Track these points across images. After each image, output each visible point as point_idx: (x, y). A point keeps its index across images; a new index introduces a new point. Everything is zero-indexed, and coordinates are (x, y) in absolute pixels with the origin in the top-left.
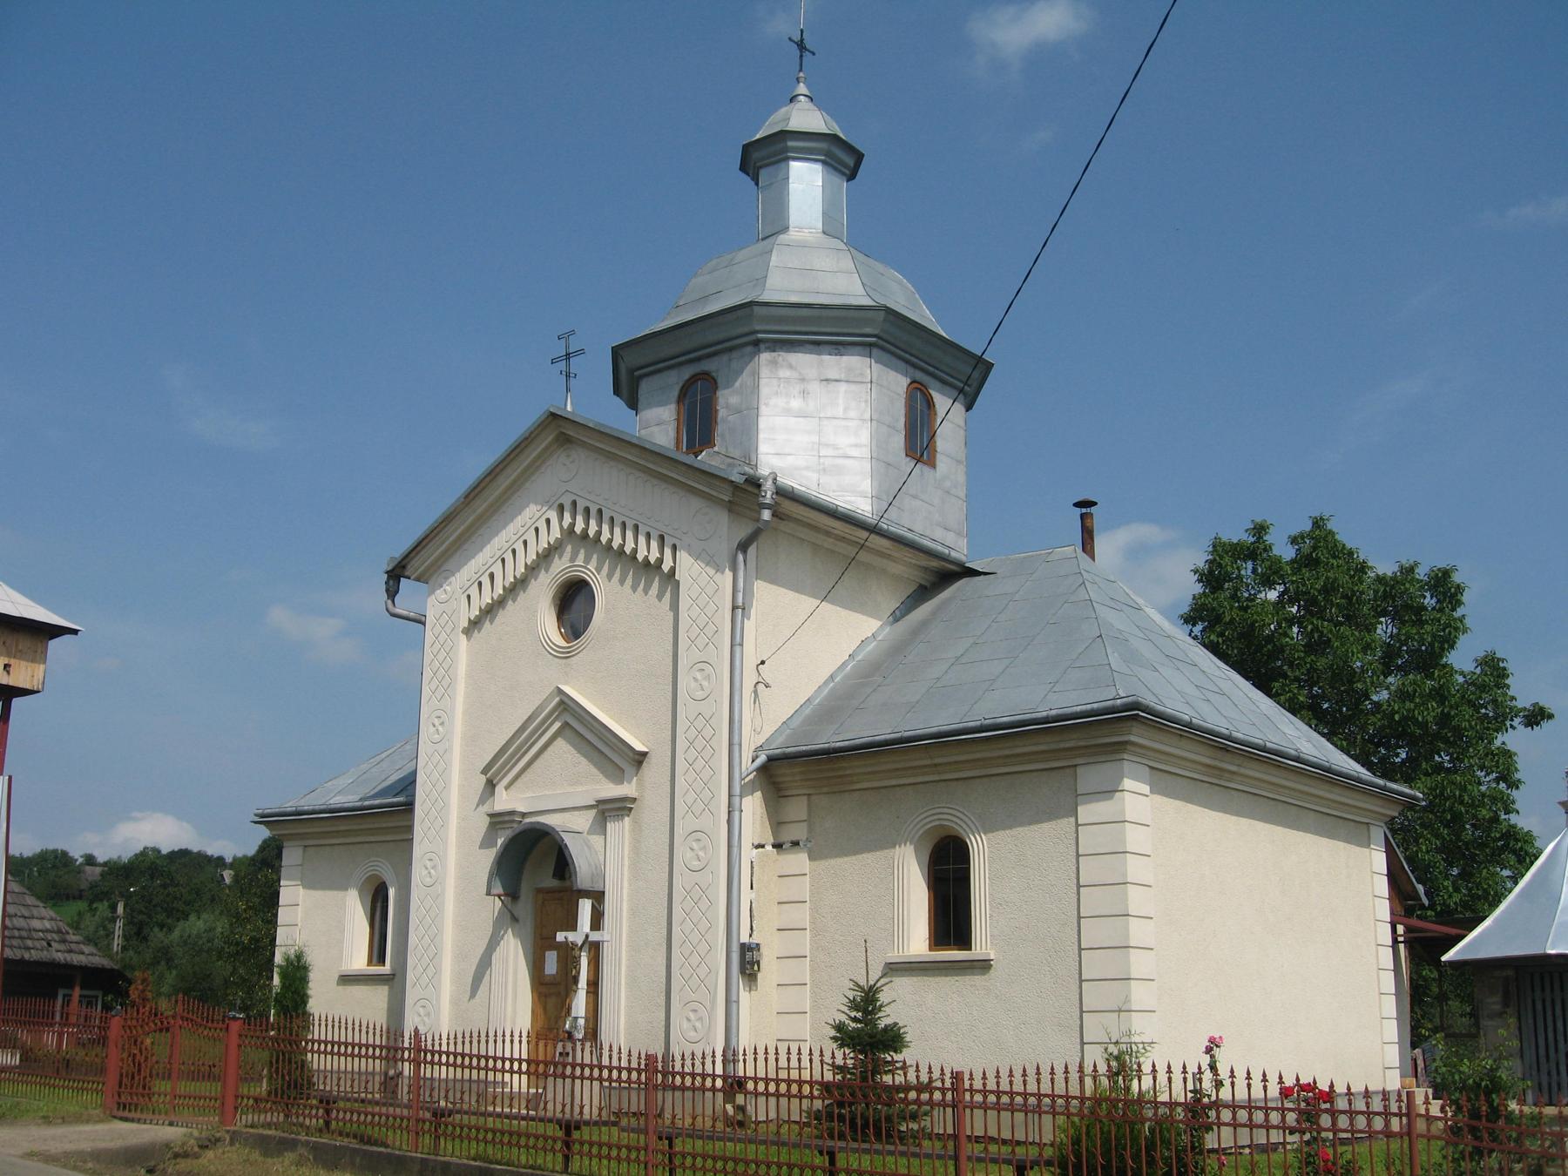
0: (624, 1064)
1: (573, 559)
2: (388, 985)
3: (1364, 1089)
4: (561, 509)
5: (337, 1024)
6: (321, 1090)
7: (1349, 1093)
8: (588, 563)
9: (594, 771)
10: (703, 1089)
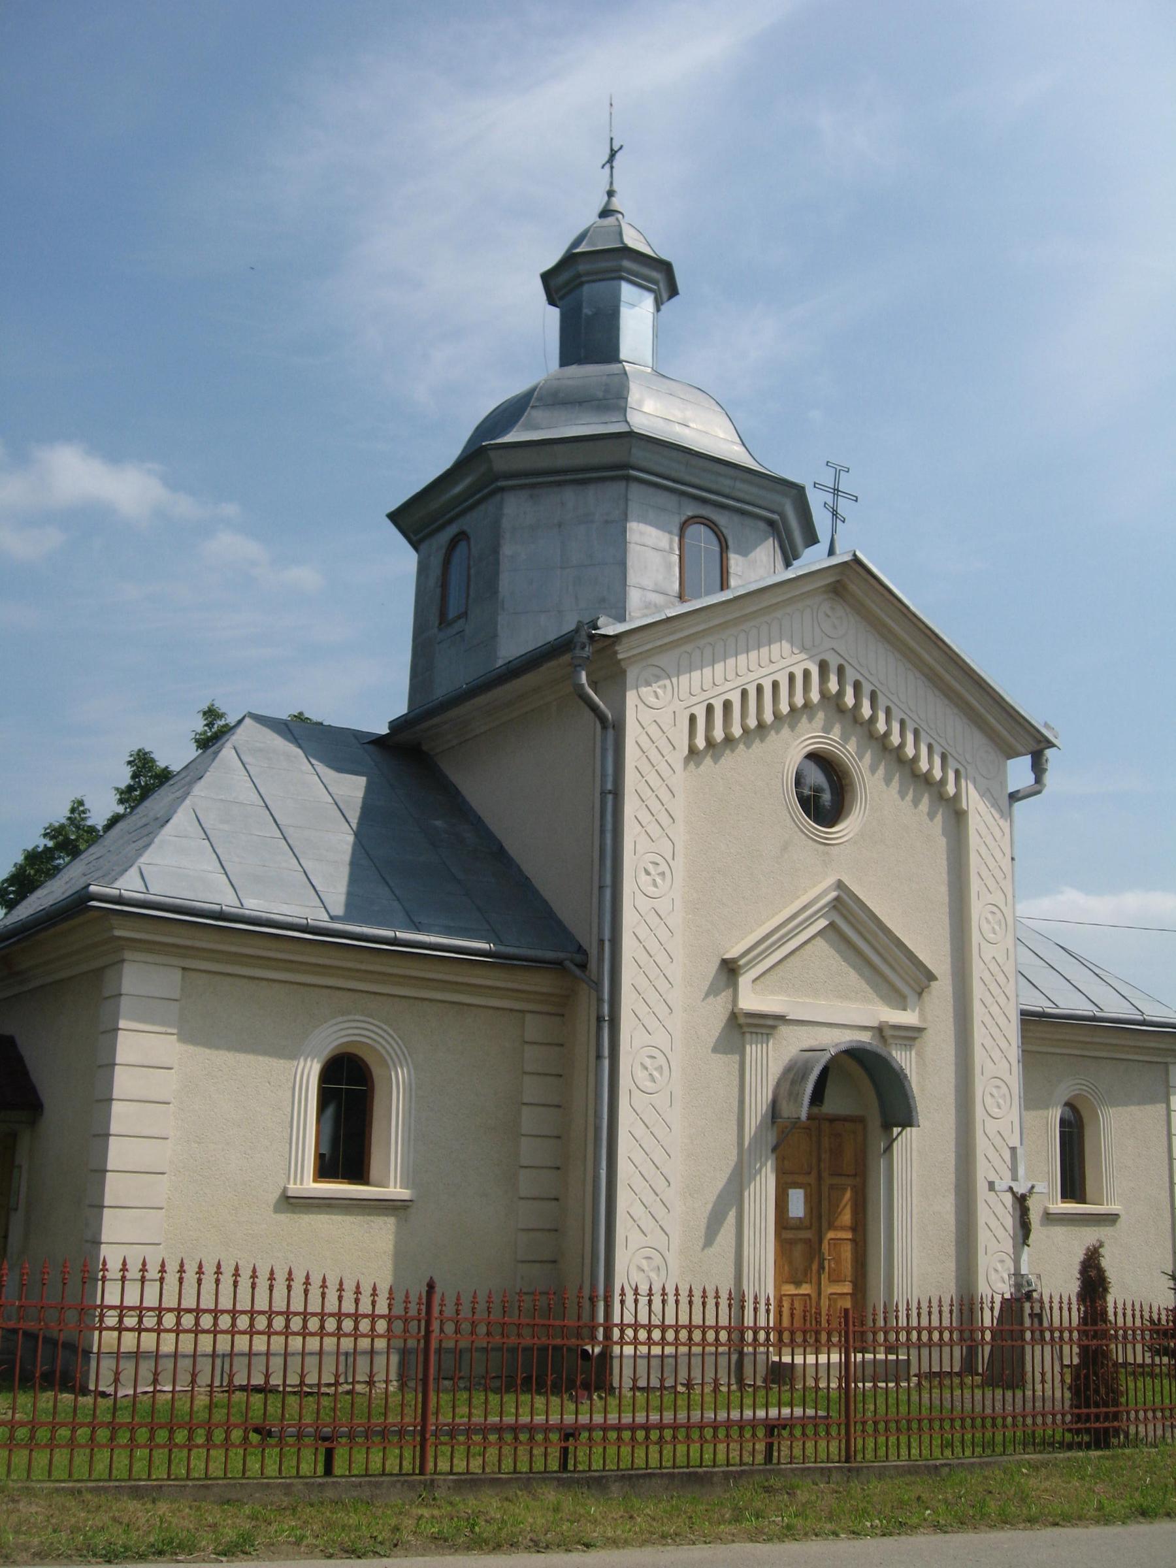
0: (348, 1307)
4: (823, 667)
5: (1065, 1307)
8: (847, 743)
9: (864, 985)
10: (930, 1344)
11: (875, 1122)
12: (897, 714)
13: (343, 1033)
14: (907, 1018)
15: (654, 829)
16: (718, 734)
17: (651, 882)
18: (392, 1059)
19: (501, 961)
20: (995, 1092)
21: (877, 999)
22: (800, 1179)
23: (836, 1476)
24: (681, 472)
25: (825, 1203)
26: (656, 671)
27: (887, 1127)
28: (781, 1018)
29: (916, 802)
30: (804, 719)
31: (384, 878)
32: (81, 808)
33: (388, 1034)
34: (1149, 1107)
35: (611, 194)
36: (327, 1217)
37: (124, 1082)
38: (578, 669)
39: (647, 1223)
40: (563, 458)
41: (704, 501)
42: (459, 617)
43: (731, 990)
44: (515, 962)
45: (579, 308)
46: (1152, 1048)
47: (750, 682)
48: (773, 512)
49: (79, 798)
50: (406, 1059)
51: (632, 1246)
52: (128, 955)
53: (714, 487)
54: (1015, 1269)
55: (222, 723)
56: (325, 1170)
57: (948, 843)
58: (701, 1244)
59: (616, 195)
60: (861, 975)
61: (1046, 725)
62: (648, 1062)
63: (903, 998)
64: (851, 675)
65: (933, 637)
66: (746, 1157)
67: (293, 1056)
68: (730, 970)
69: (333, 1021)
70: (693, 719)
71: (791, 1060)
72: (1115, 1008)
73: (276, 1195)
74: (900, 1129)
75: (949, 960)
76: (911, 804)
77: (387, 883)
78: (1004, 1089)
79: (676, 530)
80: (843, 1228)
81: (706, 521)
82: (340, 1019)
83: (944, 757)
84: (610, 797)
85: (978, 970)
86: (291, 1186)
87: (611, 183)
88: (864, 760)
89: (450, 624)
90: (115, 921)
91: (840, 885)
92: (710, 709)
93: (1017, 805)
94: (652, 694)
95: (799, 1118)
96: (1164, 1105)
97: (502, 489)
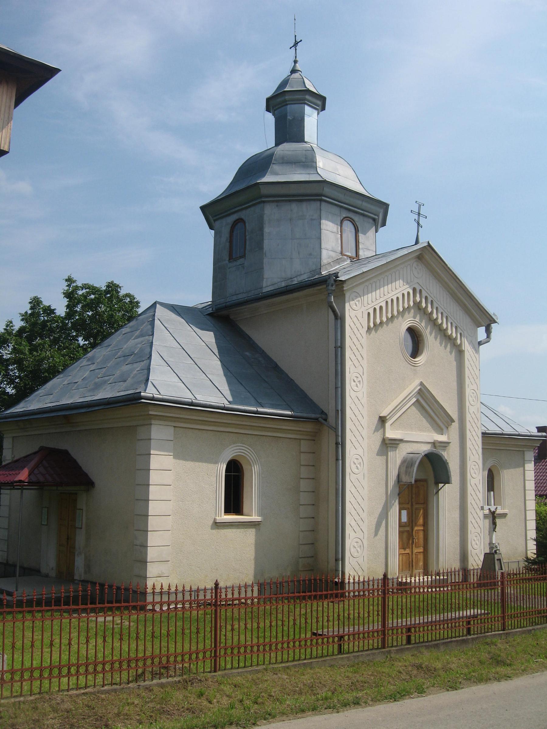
1: (414, 317)
2: (255, 528)
3: (381, 577)
4: (414, 290)
6: (457, 582)
7: (191, 591)
11: (431, 481)
12: (440, 310)
13: (237, 451)
14: (442, 438)
15: (356, 362)
16: (378, 321)
17: (356, 385)
18: (252, 461)
19: (295, 419)
20: (474, 467)
21: (433, 431)
22: (406, 506)
23: (503, 637)
24: (341, 197)
25: (414, 515)
26: (355, 294)
27: (437, 483)
28: (401, 441)
29: (446, 347)
30: (407, 313)
31: (239, 382)
32: (11, 325)
33: (251, 451)
34: (517, 469)
35: (295, 62)
36: (230, 530)
37: (154, 477)
38: (330, 295)
39: (357, 528)
40: (293, 190)
41: (349, 210)
42: (241, 257)
43: (383, 429)
44: (301, 419)
45: (286, 116)
46: (520, 445)
47: (388, 297)
48: (375, 215)
49: (10, 320)
50: (257, 461)
51: (351, 537)
52: (153, 422)
53: (347, 201)
54: (490, 541)
55: (74, 284)
56: (228, 511)
57: (456, 363)
58: (374, 535)
59: (298, 62)
60: (427, 421)
61: (494, 314)
62: (356, 461)
63: (442, 429)
64: (424, 294)
65: (455, 277)
66: (389, 498)
67: (216, 462)
68: (382, 420)
69: (231, 447)
70: (369, 314)
71: (404, 458)
72: (508, 430)
73: (211, 522)
74: (443, 485)
75: (457, 413)
76: (444, 348)
77: (242, 384)
78: (477, 466)
79: (339, 223)
80: (420, 526)
81: (351, 220)
82: (233, 446)
83: (456, 328)
84: (339, 349)
85: (468, 417)
86: (217, 518)
87: (296, 57)
88: (428, 330)
89: (236, 260)
90: (151, 408)
91: (421, 384)
92: (375, 309)
93: (481, 347)
94: (355, 304)
95: (411, 482)
96: (523, 468)
97: (264, 202)
